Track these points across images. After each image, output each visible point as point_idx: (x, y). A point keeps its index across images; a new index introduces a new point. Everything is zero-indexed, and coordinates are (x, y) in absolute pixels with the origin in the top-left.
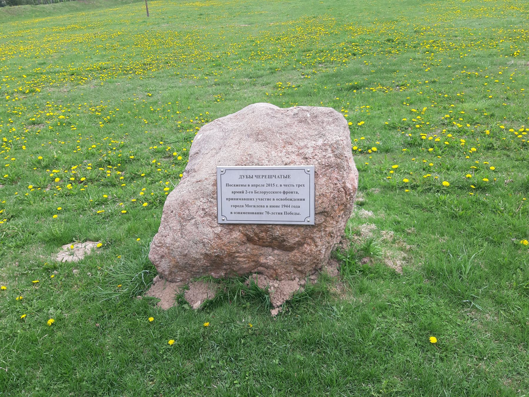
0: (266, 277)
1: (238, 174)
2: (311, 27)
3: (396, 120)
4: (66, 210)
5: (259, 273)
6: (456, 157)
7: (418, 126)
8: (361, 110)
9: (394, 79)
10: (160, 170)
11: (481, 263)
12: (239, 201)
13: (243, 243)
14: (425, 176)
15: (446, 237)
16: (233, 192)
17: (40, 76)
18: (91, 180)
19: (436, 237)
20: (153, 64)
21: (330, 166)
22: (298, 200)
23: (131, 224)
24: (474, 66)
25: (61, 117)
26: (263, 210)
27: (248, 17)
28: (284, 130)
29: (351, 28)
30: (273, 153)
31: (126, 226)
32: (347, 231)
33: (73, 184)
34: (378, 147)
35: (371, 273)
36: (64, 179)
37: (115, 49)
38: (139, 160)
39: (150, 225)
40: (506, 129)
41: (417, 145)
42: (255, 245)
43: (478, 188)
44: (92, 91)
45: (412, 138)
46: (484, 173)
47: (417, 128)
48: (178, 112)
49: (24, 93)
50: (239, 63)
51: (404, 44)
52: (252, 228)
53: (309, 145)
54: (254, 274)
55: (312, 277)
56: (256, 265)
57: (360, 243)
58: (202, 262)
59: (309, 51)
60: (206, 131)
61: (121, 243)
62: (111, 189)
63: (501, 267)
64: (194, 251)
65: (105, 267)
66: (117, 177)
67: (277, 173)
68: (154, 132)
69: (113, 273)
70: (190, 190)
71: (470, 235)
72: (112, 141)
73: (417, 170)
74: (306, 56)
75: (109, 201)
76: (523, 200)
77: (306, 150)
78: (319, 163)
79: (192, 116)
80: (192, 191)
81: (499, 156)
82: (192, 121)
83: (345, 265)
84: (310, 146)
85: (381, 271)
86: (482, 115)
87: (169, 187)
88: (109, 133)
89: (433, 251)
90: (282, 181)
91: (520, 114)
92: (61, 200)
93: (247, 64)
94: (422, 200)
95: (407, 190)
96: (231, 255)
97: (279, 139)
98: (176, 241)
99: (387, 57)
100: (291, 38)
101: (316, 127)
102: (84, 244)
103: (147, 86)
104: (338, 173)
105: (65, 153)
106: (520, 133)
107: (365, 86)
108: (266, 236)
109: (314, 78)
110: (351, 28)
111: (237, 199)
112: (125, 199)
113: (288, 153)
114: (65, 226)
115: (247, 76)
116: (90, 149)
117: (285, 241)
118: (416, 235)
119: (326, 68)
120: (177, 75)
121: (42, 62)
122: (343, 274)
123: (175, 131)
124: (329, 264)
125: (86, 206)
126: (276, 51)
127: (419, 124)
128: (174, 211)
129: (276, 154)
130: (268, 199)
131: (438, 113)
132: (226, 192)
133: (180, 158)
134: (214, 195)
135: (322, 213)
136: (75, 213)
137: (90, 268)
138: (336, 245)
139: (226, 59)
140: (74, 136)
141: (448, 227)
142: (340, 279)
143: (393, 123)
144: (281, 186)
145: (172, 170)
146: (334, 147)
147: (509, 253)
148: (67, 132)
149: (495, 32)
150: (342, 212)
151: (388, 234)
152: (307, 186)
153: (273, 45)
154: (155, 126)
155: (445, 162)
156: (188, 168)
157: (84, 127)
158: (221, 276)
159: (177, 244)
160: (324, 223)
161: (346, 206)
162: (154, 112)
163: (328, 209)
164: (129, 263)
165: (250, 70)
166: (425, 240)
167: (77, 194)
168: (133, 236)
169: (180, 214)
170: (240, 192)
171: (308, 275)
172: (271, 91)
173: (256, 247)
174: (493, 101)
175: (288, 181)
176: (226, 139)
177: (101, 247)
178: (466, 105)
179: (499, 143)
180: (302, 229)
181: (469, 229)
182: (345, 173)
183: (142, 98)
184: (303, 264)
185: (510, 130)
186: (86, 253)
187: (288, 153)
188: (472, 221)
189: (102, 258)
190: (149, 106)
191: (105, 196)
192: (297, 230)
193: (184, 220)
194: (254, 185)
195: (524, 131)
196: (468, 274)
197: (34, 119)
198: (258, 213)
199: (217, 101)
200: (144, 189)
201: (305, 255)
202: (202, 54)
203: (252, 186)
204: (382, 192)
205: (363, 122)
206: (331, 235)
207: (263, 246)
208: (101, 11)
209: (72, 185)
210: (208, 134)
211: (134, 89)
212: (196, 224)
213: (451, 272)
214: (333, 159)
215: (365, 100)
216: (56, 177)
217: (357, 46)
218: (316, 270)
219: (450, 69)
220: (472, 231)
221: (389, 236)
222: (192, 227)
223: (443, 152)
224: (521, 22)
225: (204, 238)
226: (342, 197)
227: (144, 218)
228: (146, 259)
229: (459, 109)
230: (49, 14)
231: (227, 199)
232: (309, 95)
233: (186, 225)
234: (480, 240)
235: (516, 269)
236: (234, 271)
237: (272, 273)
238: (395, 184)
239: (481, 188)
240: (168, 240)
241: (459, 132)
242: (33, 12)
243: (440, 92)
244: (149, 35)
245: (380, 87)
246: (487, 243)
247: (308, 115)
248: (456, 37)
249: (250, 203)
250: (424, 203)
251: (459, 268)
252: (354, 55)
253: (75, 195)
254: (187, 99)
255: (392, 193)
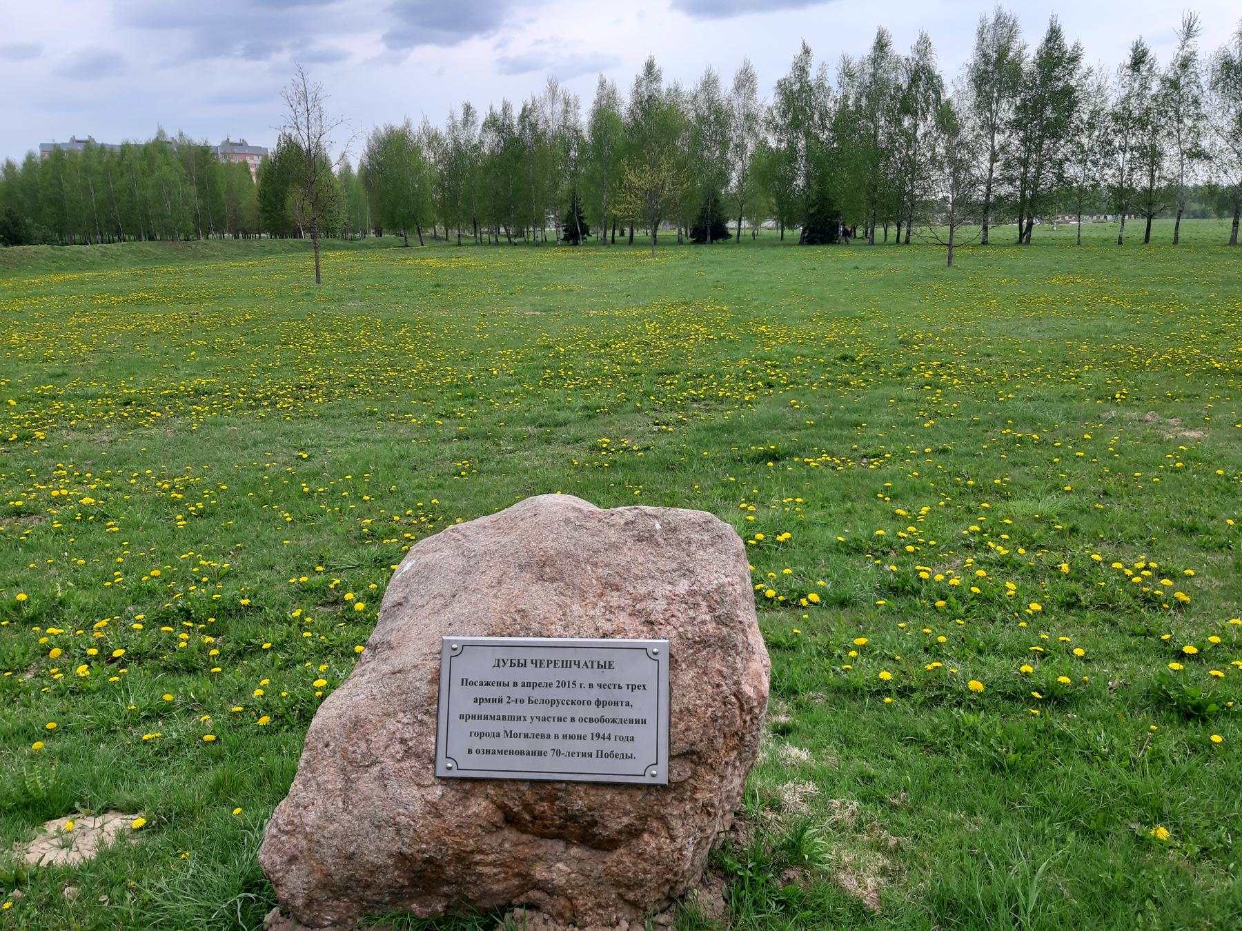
0: (546, 916)
1: (491, 656)
2: (679, 323)
3: (862, 533)
4: (66, 730)
5: (532, 906)
6: (998, 623)
7: (910, 548)
8: (783, 505)
9: (855, 440)
10: (309, 634)
11: (1062, 882)
12: (490, 722)
13: (493, 828)
14: (929, 667)
15: (980, 818)
16: (476, 701)
17: (49, 402)
18: (138, 656)
19: (956, 817)
20: (319, 388)
21: (704, 643)
22: (631, 721)
23: (223, 769)
24: (1031, 421)
25: (87, 500)
26: (546, 745)
27: (543, 294)
28: (603, 558)
29: (763, 328)
30: (575, 607)
31: (210, 776)
32: (748, 798)
33: (93, 663)
34: (823, 593)
35: (805, 908)
36: (72, 651)
37: (234, 352)
38: (260, 609)
39: (270, 774)
40: (1105, 562)
41: (909, 592)
42: (523, 832)
43: (1049, 699)
44: (169, 444)
45: (899, 576)
46: (1060, 662)
47: (908, 553)
48: (367, 498)
49: (6, 441)
50: (517, 394)
51: (878, 367)
52: (518, 790)
53: (658, 593)
54: (517, 910)
55: (662, 919)
56: (522, 886)
57: (779, 831)
58: (389, 876)
59: (672, 373)
60: (425, 553)
61: (194, 818)
62: (185, 678)
63: (1109, 894)
64: (372, 848)
65: (145, 883)
66: (204, 649)
67: (583, 656)
68: (304, 543)
69: (165, 898)
70: (375, 691)
71: (1035, 814)
72: (202, 562)
73: (911, 650)
74: (664, 384)
75: (174, 710)
76: (1151, 731)
77: (650, 605)
78: (680, 636)
79: (399, 508)
80: (379, 696)
81: (1092, 624)
82: (397, 518)
83: (743, 888)
84: (662, 593)
85: (829, 903)
86: (1050, 528)
87: (326, 678)
88: (197, 543)
89: (952, 853)
90: (595, 676)
91: (1135, 529)
92: (59, 704)
93: (534, 395)
94: (923, 723)
95: (888, 700)
96: (462, 858)
97: (590, 578)
98: (331, 819)
99: (840, 393)
100: (633, 345)
101: (674, 552)
102: (100, 820)
103: (299, 437)
104: (723, 659)
105: (84, 588)
106: (1138, 573)
107: (793, 455)
108: (552, 810)
109: (680, 432)
110: (763, 328)
111: (486, 718)
112: (217, 705)
113: (609, 609)
114: (58, 771)
115: (533, 422)
116: (145, 578)
117: (595, 823)
118: (911, 812)
119: (709, 411)
120: (372, 413)
121: (59, 371)
122: (738, 911)
123: (354, 542)
124: (705, 883)
125: (117, 721)
126: (600, 370)
127: (913, 544)
128: (332, 744)
129: (582, 612)
130: (560, 719)
131: (955, 520)
132: (461, 700)
133: (360, 606)
134: (431, 707)
135: (687, 755)
136: (89, 738)
137: (108, 884)
138: (722, 835)
139: (488, 382)
140: (112, 546)
141: (984, 792)
142: (730, 924)
143: (855, 540)
144: (591, 686)
145: (338, 635)
146: (716, 599)
147: (1126, 860)
148: (96, 536)
149: (1072, 348)
150: (734, 754)
151: (846, 808)
152: (652, 687)
153: (593, 356)
154: (310, 529)
155: (974, 635)
156: (375, 637)
157: (137, 525)
158: (435, 912)
159: (331, 828)
160: (691, 781)
161: (742, 739)
162: (309, 496)
163: (701, 747)
164: (209, 875)
165: (541, 409)
166: (931, 823)
167: (99, 689)
168: (225, 802)
169: (345, 750)
170: (494, 701)
171: (651, 912)
172: (584, 455)
173: (524, 837)
174: (1074, 498)
175: (607, 676)
176: (469, 573)
177: (141, 829)
178: (1016, 506)
179: (1091, 593)
180: (639, 796)
181: (1033, 800)
182: (738, 659)
183: (285, 464)
184: (640, 884)
185: (1115, 565)
186: (102, 842)
187: (609, 609)
188: (1037, 780)
189: (140, 858)
190: (300, 483)
191: (168, 697)
192: (625, 798)
193: (353, 765)
194: (529, 684)
195: (1146, 568)
196: (1034, 911)
197: (19, 503)
198: (534, 753)
199: (459, 475)
200: (266, 682)
201: (645, 860)
202: (433, 370)
203: (523, 685)
204: (831, 703)
205: (787, 535)
206: (707, 809)
207: (544, 836)
208: (212, 266)
209: (90, 667)
210: (428, 559)
211: (270, 441)
212: (382, 778)
213: (995, 907)
214: (711, 627)
215: (793, 485)
216: (52, 647)
217: (775, 366)
218: (670, 899)
219: (977, 424)
220: (1038, 803)
221: (847, 814)
222: (372, 786)
223: (968, 611)
224: (1126, 330)
225: (399, 814)
226: (733, 716)
227: (258, 756)
228: (251, 863)
229: (1000, 514)
230: (89, 266)
231: (461, 717)
232: (670, 468)
233: (358, 778)
234: (1058, 826)
235: (1144, 901)
236: (469, 901)
237: (564, 907)
238: (861, 682)
239: (1056, 699)
240: (311, 817)
241: (1003, 566)
242: (52, 258)
243: (958, 474)
244: (316, 324)
245: (826, 457)
246: (1073, 834)
247: (658, 526)
248: (989, 356)
249: (516, 727)
250: (927, 732)
251: (1012, 898)
252: (770, 385)
253: (94, 693)
254: (390, 467)
255: (854, 705)
